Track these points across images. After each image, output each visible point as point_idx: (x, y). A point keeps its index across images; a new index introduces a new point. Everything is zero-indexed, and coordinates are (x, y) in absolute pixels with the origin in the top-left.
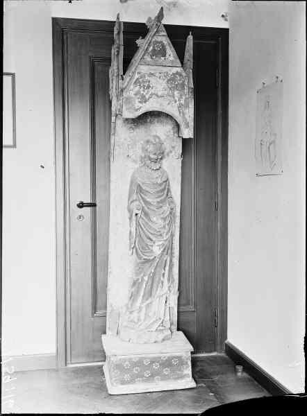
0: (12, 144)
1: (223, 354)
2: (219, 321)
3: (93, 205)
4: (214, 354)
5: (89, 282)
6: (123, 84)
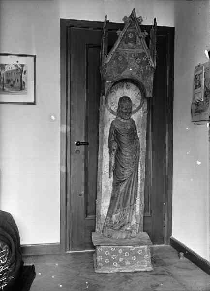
0: (33, 102)
3: (87, 144)
4: (163, 245)
5: (65, 209)
6: (106, 60)
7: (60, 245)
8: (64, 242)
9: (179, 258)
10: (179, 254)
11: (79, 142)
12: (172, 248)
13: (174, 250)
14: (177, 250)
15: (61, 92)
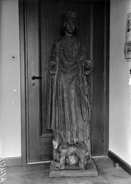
5: (25, 127)
7: (22, 159)
8: (25, 130)
9: (115, 167)
10: (115, 164)
11: (34, 77)
12: (109, 158)
13: (111, 160)
14: (114, 161)
15: (20, 23)
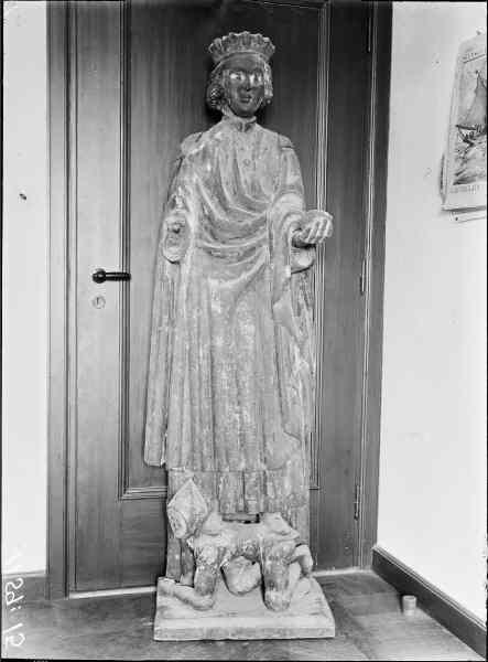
1: (369, 572)
2: (362, 508)
3: (124, 277)
4: (352, 571)
5: (116, 405)
